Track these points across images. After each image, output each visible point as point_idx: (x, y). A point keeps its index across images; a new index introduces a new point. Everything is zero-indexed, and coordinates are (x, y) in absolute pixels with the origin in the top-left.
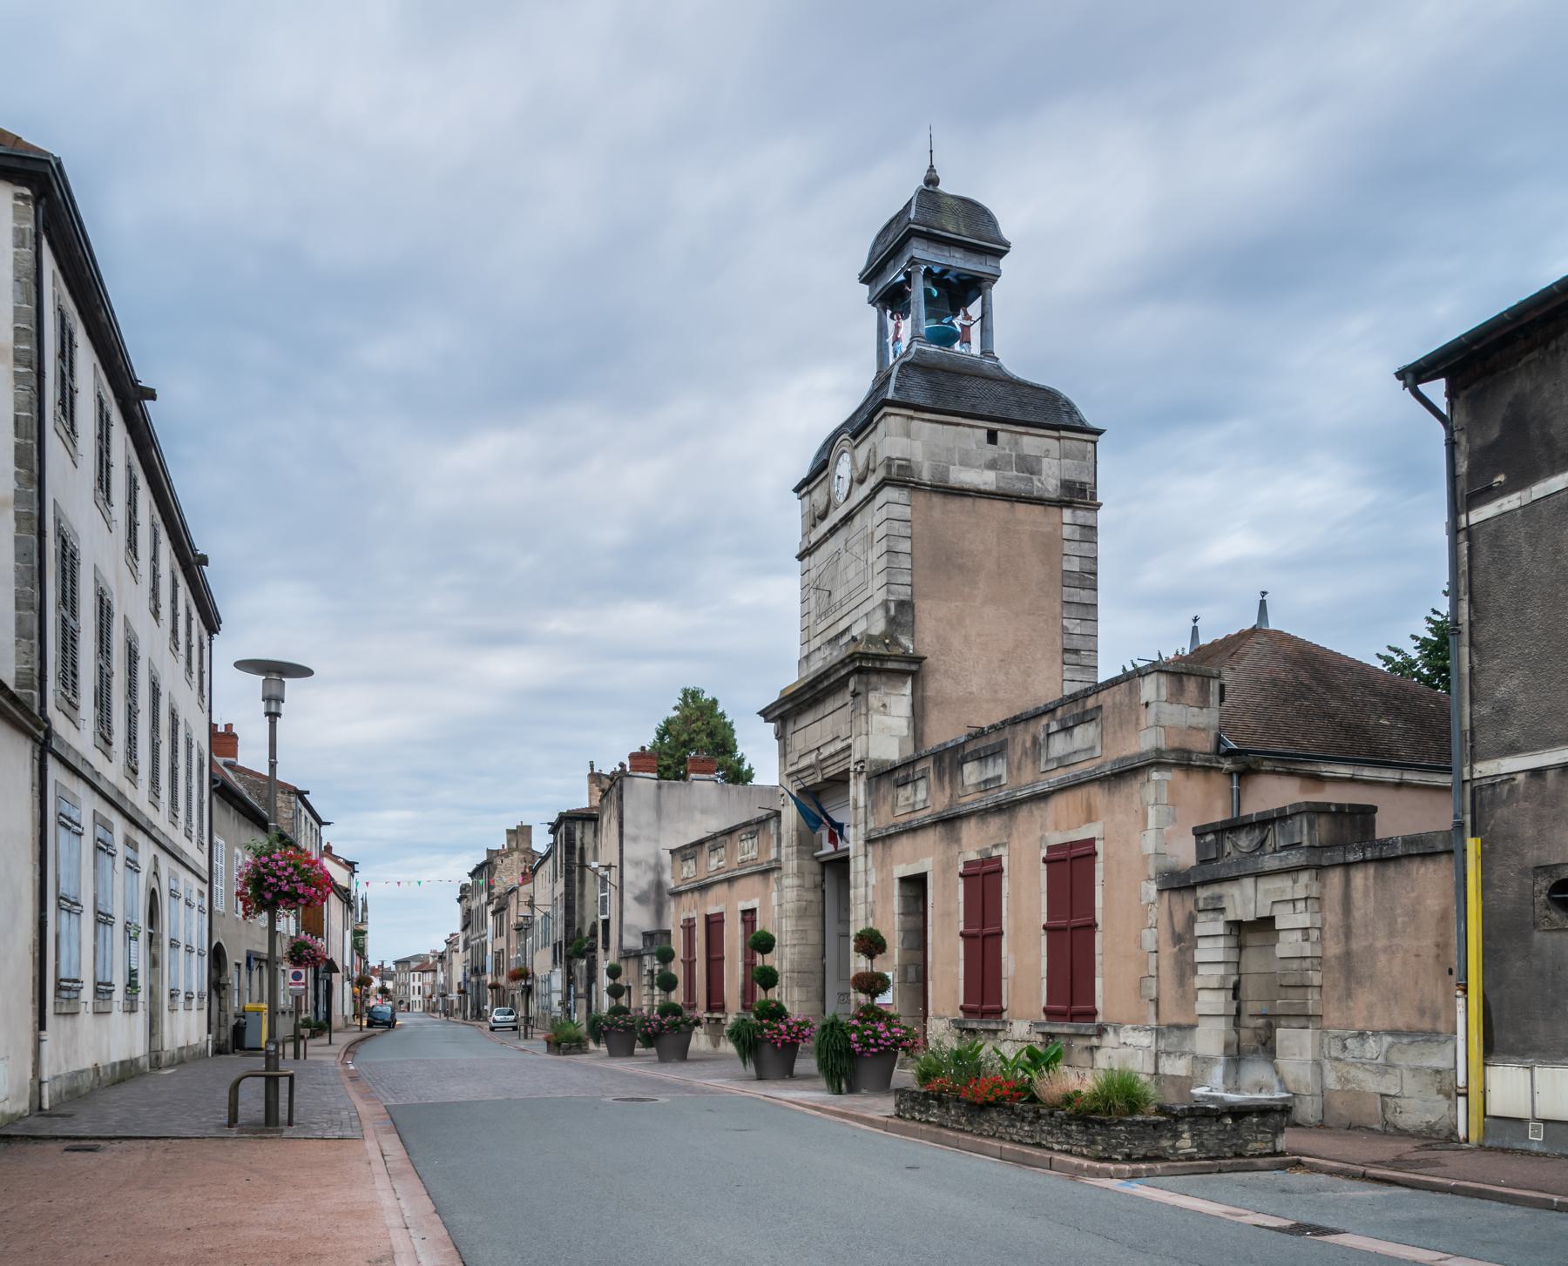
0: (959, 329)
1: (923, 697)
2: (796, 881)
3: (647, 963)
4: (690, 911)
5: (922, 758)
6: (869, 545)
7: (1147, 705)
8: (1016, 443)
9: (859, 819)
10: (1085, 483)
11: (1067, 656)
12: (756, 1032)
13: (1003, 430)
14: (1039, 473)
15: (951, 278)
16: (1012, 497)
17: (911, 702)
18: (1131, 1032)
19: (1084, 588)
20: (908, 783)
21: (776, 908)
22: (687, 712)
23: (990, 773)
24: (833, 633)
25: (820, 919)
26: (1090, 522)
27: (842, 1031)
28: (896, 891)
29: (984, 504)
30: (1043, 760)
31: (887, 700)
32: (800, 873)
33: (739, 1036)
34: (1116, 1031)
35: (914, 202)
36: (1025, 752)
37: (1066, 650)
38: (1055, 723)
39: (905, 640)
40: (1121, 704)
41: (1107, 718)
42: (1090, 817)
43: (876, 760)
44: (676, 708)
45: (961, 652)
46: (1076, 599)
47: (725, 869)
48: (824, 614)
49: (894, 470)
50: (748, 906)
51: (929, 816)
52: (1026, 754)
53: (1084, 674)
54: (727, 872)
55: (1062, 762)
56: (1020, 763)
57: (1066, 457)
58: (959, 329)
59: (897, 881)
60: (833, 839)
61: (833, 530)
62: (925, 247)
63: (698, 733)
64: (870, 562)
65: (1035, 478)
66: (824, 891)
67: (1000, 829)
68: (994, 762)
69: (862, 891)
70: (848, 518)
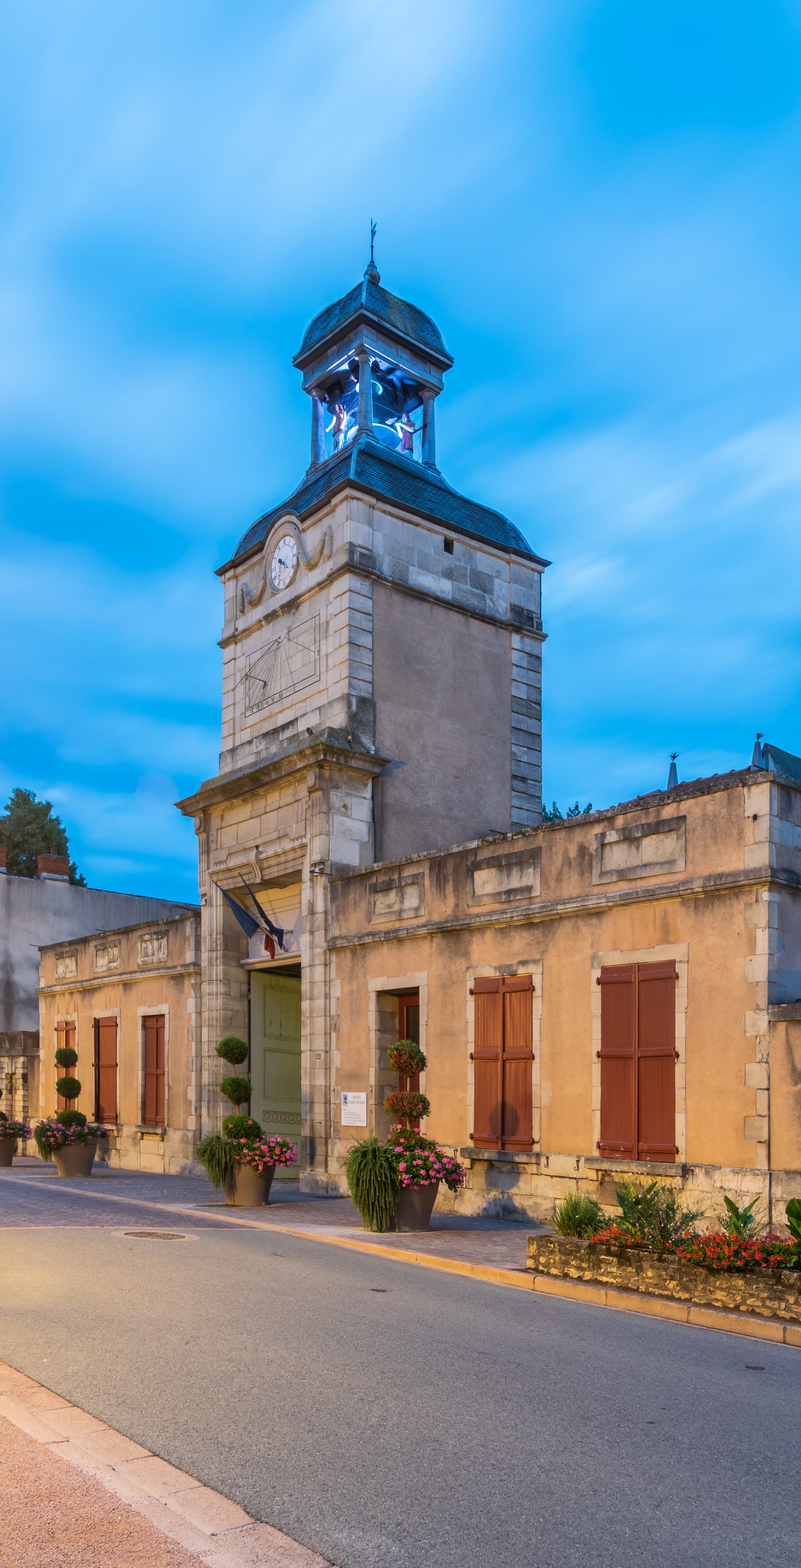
0: (400, 435)
1: (382, 802)
2: (221, 988)
3: (5, 1066)
4: (67, 1013)
5: (413, 862)
6: (323, 635)
7: (755, 817)
8: (471, 557)
9: (316, 924)
10: (532, 612)
11: (515, 782)
12: (233, 1153)
13: (459, 541)
14: (491, 592)
15: (395, 379)
16: (467, 611)
17: (371, 806)
18: (731, 1175)
19: (530, 717)
20: (390, 889)
21: (194, 1016)
22: (20, 812)
23: (516, 881)
24: (268, 727)
25: (247, 1030)
26: (536, 652)
27: (387, 1159)
28: (372, 1006)
29: (441, 613)
30: (596, 872)
31: (348, 800)
32: (226, 980)
33: (213, 1156)
34: (707, 1173)
35: (364, 287)
36: (567, 862)
37: (514, 777)
38: (614, 833)
39: (366, 740)
40: (715, 815)
41: (694, 830)
42: (667, 936)
43: (337, 863)
44: (7, 808)
45: (418, 762)
46: (524, 727)
47: (120, 971)
48: (258, 706)
49: (356, 557)
50: (154, 1011)
51: (424, 926)
52: (570, 865)
53: (530, 803)
54: (121, 974)
55: (623, 875)
56: (560, 873)
57: (516, 582)
58: (400, 435)
59: (373, 996)
60: (269, 945)
61: (271, 617)
62: (375, 338)
63: (33, 836)
64: (323, 653)
65: (487, 596)
66: (249, 1002)
67: (530, 945)
68: (521, 870)
69: (320, 1003)
70: (292, 605)
